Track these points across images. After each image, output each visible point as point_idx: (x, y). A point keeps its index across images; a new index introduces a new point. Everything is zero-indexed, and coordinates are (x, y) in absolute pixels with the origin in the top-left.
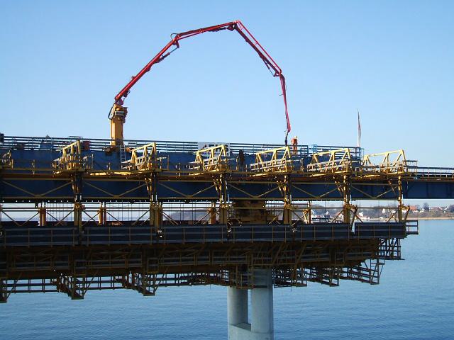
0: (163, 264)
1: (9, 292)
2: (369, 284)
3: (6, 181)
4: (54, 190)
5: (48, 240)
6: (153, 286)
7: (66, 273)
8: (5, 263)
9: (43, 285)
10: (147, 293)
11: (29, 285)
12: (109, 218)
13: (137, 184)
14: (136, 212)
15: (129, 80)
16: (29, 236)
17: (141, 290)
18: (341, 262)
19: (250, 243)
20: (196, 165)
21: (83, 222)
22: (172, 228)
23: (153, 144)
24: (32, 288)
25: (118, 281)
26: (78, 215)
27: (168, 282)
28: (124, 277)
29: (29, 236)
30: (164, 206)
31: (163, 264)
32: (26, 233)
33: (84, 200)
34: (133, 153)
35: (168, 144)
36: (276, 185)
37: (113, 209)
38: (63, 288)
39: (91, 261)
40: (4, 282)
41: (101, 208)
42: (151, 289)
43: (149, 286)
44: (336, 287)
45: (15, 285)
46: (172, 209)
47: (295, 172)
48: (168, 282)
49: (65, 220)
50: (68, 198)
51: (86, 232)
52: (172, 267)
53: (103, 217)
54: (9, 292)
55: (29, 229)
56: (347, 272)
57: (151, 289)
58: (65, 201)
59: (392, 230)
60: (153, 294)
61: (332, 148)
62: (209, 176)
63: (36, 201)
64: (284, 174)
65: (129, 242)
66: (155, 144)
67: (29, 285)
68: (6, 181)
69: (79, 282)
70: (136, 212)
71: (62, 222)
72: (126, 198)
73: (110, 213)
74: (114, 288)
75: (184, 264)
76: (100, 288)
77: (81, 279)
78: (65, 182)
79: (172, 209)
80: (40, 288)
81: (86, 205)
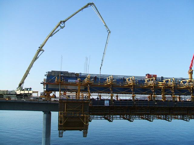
0: (136, 113)
1: (92, 119)
5: (187, 105)
6: (132, 119)
7: (107, 114)
9: (101, 117)
10: (131, 121)
12: (102, 98)
13: (129, 89)
14: (127, 97)
15: (191, 62)
17: (129, 120)
18: (172, 114)
19: (182, 107)
20: (145, 83)
23: (174, 79)
24: (98, 118)
25: (122, 117)
27: (117, 118)
28: (123, 116)
31: (136, 113)
34: (146, 80)
35: (137, 77)
36: (170, 90)
37: (104, 96)
38: (106, 119)
41: (117, 95)
42: (132, 120)
43: (131, 119)
44: (170, 122)
45: (113, 117)
46: (139, 97)
47: (156, 85)
48: (98, 118)
52: (138, 114)
53: (117, 99)
54: (92, 119)
56: (151, 119)
57: (132, 120)
58: (129, 94)
60: (112, 121)
61: (169, 78)
62: (150, 87)
63: (98, 93)
64: (172, 87)
65: (148, 106)
67: (97, 117)
69: (111, 117)
70: (127, 97)
74: (121, 119)
75: (177, 113)
76: (97, 119)
77: (112, 116)
78: (108, 88)
79: (139, 97)
80: (100, 118)
81: (91, 94)
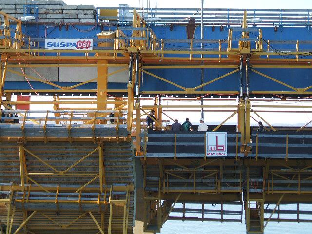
2: (297, 223)
3: (256, 69)
4: (220, 78)
8: (260, 180)
11: (279, 212)
16: (287, 145)
21: (252, 128)
22: (184, 135)
26: (135, 114)
29: (287, 145)
30: (95, 106)
32: (283, 141)
33: (251, 96)
39: (272, 181)
40: (265, 206)
49: (224, 124)
50: (171, 93)
51: (254, 141)
55: (175, 135)
59: (291, 145)
66: (203, 21)
67: (203, 211)
68: (256, 69)
71: (305, 127)
72: (209, 92)
73: (165, 112)
